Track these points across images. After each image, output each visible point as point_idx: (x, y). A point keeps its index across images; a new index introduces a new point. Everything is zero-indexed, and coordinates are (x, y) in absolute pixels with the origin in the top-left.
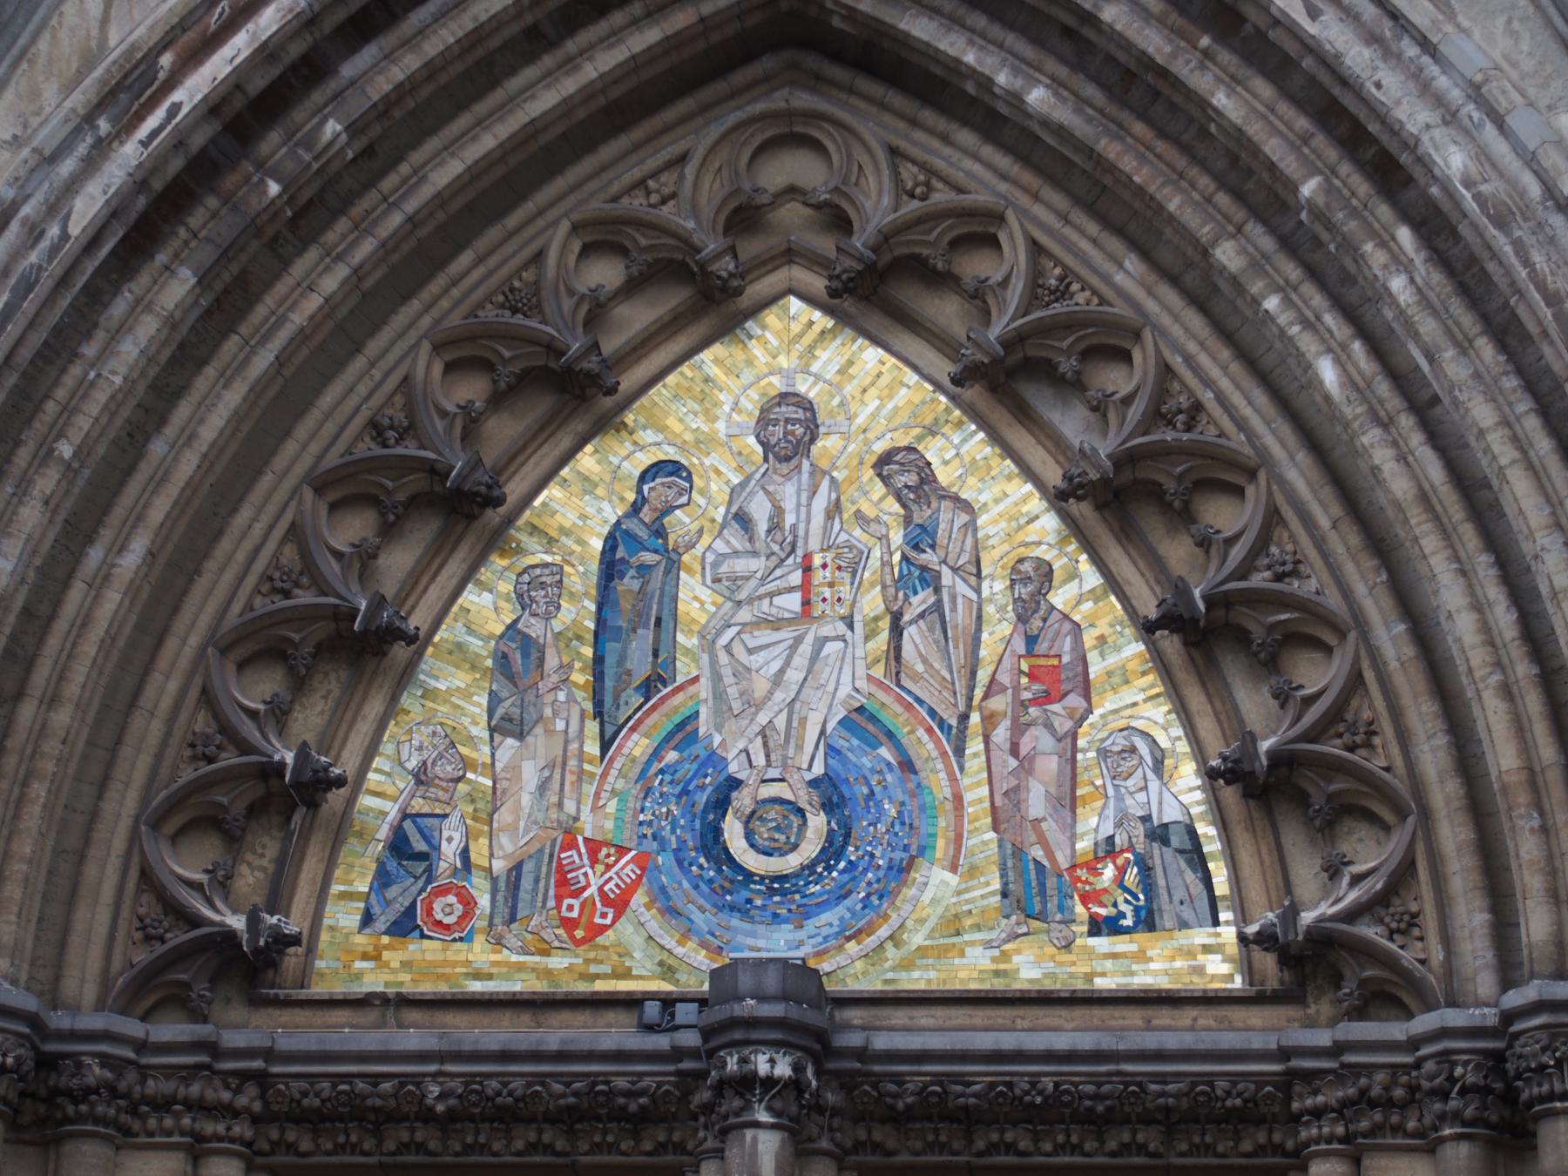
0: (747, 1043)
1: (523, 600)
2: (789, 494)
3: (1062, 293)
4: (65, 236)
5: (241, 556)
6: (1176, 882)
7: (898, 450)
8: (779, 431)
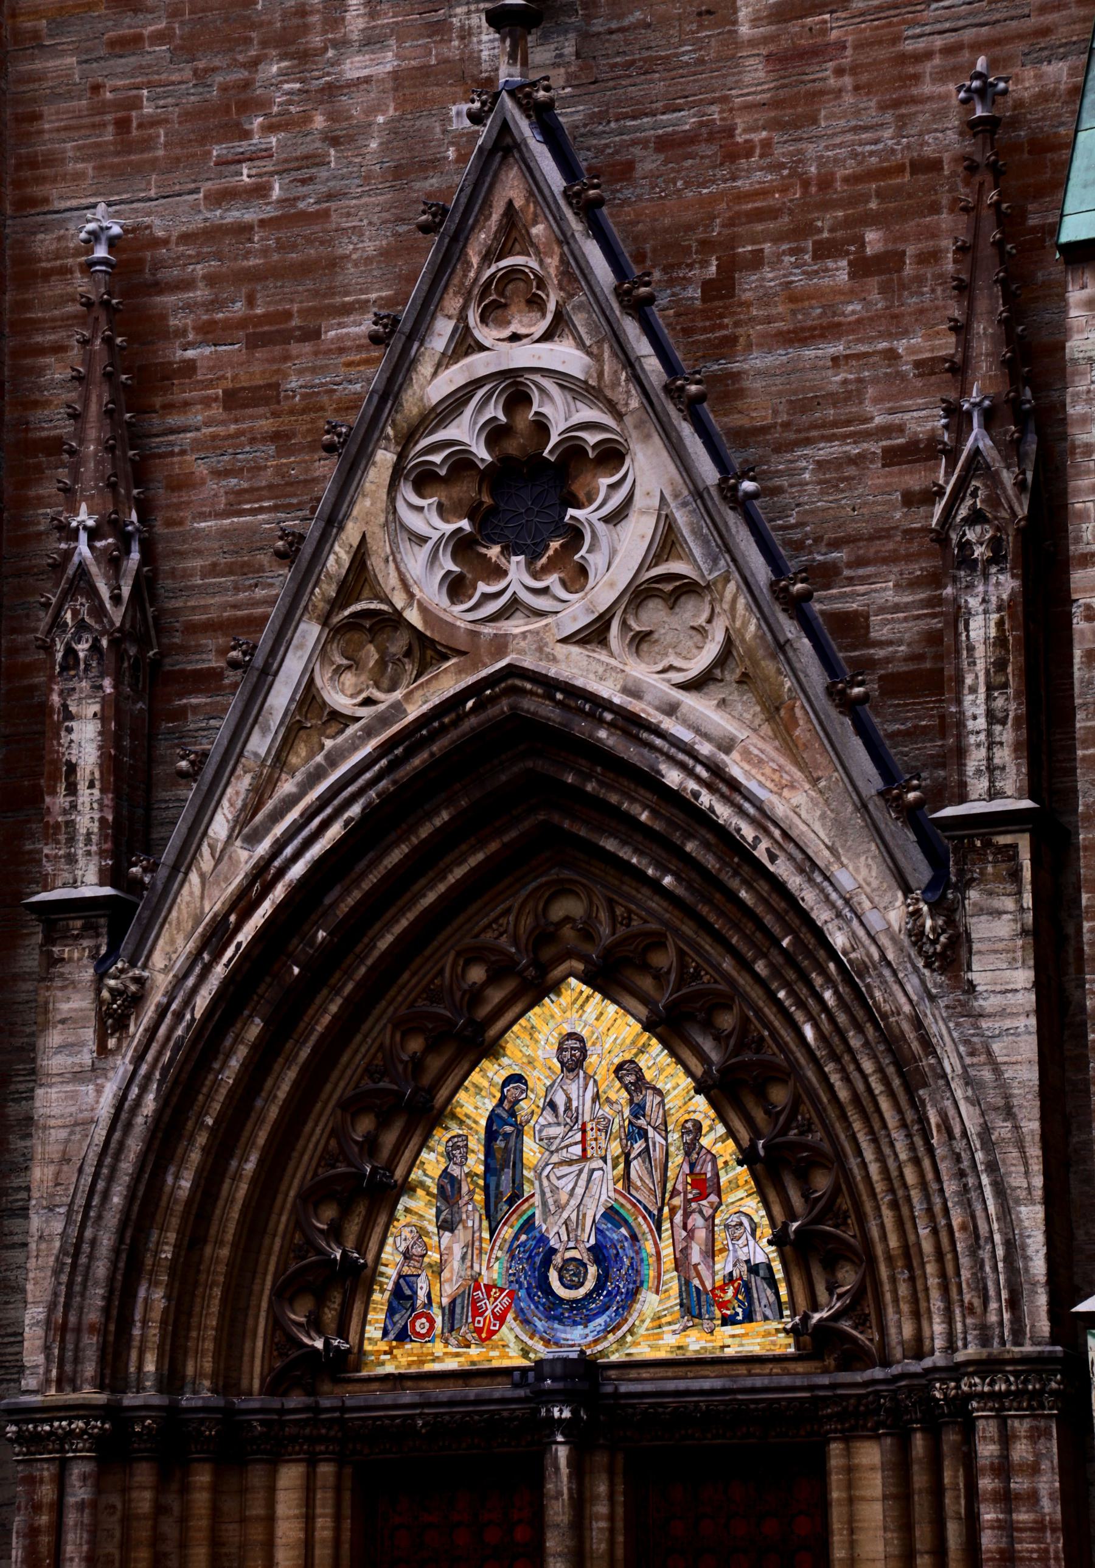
0: (549, 1402)
1: (450, 1157)
2: (573, 1089)
3: (696, 976)
4: (193, 1019)
5: (311, 1146)
6: (762, 1295)
7: (625, 1062)
8: (568, 1054)
